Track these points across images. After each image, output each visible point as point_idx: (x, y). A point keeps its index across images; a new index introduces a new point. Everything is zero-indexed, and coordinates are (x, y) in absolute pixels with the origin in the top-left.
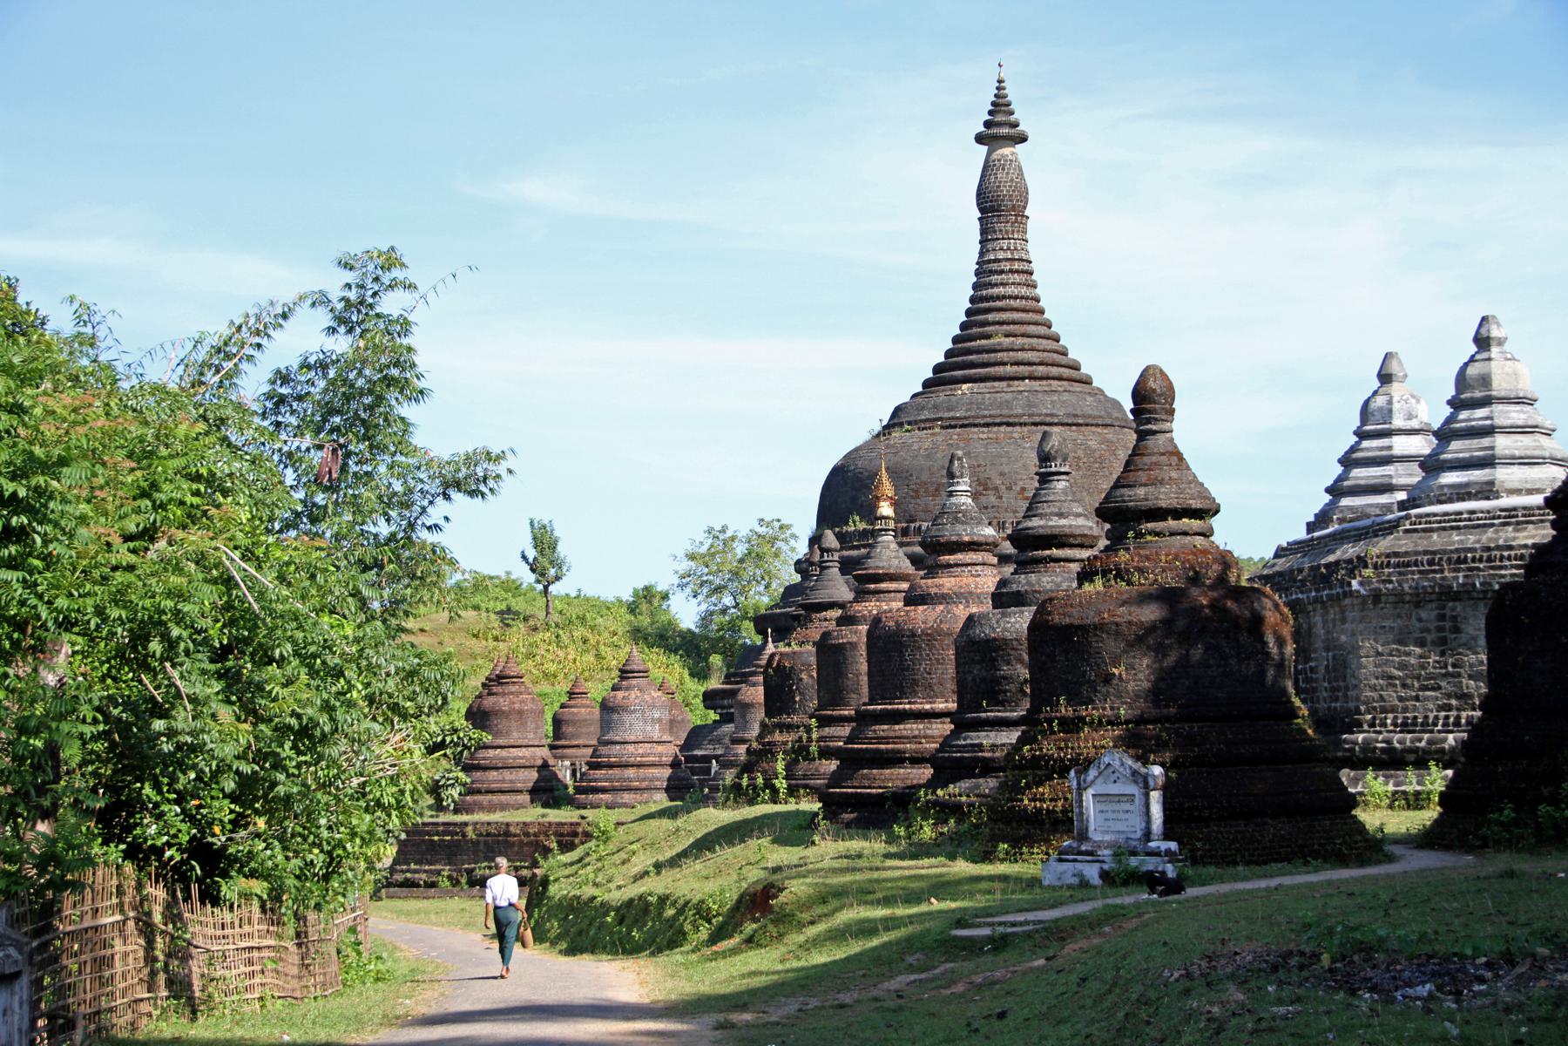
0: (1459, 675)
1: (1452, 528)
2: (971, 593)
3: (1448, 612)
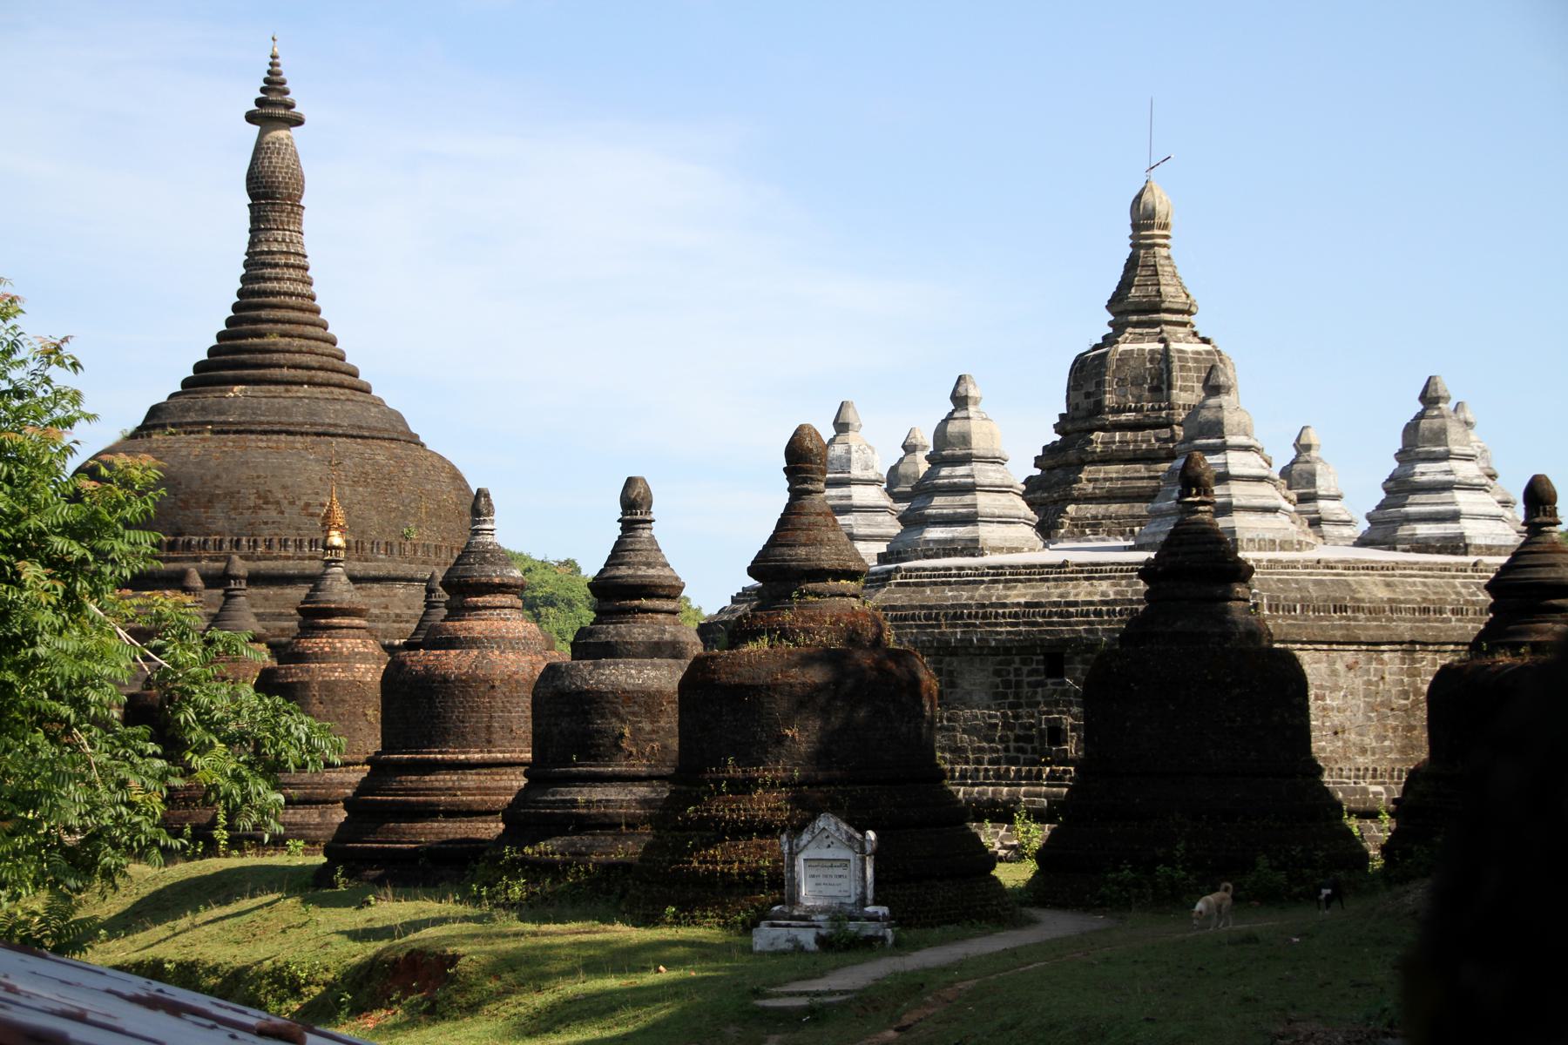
0: (954, 729)
1: (943, 583)
2: (502, 637)
3: (944, 666)
